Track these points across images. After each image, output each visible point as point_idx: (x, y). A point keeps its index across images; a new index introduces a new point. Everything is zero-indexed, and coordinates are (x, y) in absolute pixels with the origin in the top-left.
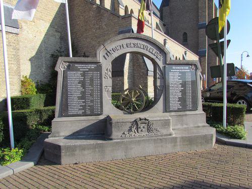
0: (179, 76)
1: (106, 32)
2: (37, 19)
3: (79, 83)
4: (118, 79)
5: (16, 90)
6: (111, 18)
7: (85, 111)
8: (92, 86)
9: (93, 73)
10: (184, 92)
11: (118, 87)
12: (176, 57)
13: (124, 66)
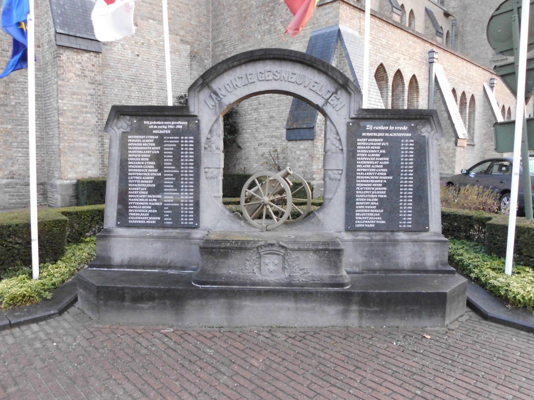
0: (382, 147)
2: (142, 19)
3: (150, 160)
5: (94, 165)
8: (178, 167)
11: (301, 164)
12: (464, 93)
13: (380, 109)
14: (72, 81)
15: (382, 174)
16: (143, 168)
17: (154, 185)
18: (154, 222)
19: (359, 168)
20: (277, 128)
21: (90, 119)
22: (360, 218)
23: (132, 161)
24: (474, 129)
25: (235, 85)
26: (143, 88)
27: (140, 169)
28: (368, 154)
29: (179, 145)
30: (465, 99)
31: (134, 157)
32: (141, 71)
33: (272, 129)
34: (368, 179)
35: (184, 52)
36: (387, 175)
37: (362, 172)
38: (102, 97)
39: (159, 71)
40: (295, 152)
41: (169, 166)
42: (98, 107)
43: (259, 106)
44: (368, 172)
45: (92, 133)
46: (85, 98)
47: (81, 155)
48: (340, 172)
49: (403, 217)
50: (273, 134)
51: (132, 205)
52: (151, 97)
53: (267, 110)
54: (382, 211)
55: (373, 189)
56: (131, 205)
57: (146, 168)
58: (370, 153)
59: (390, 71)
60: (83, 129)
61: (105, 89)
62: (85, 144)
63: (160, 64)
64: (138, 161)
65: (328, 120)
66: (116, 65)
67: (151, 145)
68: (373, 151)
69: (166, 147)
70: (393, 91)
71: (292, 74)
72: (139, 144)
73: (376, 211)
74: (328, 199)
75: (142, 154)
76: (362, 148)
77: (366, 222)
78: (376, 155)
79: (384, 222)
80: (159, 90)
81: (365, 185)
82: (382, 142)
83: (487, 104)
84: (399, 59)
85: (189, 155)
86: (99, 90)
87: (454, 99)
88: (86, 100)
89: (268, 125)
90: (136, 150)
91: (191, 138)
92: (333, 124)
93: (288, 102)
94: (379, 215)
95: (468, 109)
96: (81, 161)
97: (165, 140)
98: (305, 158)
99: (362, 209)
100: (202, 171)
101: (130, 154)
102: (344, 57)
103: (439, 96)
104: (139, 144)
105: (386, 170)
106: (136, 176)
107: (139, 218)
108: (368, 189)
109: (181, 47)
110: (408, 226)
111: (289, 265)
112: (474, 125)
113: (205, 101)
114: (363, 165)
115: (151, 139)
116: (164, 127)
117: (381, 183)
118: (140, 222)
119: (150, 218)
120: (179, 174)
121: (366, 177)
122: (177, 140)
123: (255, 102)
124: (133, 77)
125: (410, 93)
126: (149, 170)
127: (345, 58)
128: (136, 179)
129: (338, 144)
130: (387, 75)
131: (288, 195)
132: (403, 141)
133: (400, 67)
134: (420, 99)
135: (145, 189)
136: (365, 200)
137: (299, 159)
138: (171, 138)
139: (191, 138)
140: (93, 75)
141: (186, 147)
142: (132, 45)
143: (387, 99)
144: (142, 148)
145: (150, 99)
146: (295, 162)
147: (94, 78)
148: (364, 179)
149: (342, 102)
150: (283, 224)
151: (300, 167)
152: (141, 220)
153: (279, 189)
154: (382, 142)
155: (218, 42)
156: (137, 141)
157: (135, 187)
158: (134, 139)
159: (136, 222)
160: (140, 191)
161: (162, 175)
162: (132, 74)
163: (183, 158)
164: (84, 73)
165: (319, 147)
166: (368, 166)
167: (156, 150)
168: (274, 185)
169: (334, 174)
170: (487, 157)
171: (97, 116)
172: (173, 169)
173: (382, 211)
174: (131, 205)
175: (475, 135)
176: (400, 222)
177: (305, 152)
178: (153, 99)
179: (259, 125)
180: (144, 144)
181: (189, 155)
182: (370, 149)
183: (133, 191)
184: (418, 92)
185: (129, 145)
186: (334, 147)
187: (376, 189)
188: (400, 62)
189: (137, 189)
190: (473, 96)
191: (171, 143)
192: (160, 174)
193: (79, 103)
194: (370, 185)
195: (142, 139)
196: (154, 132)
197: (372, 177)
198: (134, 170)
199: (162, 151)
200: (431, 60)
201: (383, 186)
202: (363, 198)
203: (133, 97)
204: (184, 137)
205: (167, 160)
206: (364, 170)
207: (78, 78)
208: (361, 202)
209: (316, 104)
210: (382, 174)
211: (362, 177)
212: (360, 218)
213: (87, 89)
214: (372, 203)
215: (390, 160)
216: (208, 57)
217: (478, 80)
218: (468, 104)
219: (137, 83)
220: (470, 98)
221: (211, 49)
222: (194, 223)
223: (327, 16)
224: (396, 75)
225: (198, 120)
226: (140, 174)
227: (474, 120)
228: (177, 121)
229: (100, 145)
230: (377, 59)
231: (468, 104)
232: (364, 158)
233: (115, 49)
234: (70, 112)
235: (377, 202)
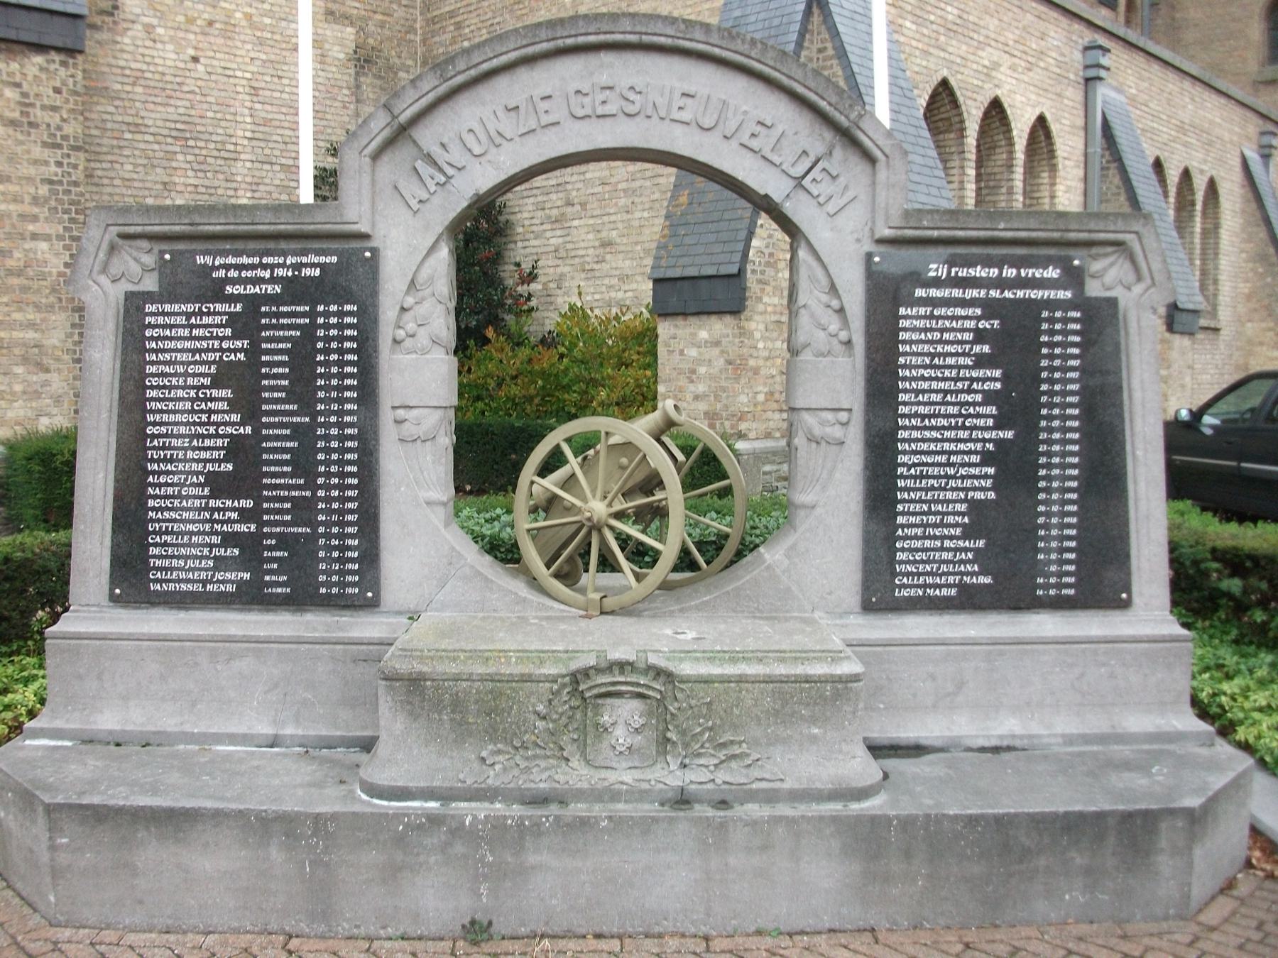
0: (980, 336)
3: (217, 383)
4: (704, 334)
5: (58, 400)
8: (307, 405)
9: (313, 315)
11: (701, 388)
12: (1186, 175)
17: (230, 467)
18: (231, 588)
19: (905, 404)
20: (624, 278)
21: (47, 256)
22: (910, 568)
23: (158, 387)
24: (1216, 282)
25: (493, 134)
26: (209, 160)
27: (183, 412)
28: (932, 356)
29: (309, 333)
30: (1191, 190)
32: (205, 106)
33: (606, 281)
34: (936, 440)
35: (336, 48)
36: (997, 427)
37: (916, 415)
38: (81, 189)
39: (258, 106)
40: (682, 353)
42: (72, 220)
43: (569, 210)
44: (935, 416)
45: (52, 299)
46: (32, 190)
47: (19, 370)
48: (843, 416)
49: (1050, 562)
50: (613, 294)
51: (160, 533)
52: (234, 185)
53: (591, 221)
54: (981, 543)
55: (951, 471)
56: (154, 532)
57: (202, 411)
58: (939, 355)
59: (969, 102)
60: (25, 289)
61: (92, 165)
62: (31, 335)
63: (263, 85)
64: (177, 387)
65: (803, 244)
66: (128, 88)
68: (948, 348)
69: (270, 340)
70: (980, 164)
71: (683, 94)
72: (181, 332)
73: (961, 543)
74: (804, 506)
75: (190, 363)
76: (915, 337)
77: (930, 580)
78: (962, 361)
79: (986, 580)
80: (258, 165)
81: (924, 459)
82: (978, 319)
83: (1254, 206)
84: (996, 66)
86: (75, 167)
87: (1159, 190)
89: (596, 267)
90: (170, 350)
91: (348, 308)
92: (818, 258)
93: (657, 196)
94: (970, 555)
95: (1198, 219)
96: (18, 388)
97: (266, 315)
98: (715, 371)
99: (916, 537)
100: (386, 417)
101: (153, 363)
102: (831, 58)
103: (1117, 180)
104: (181, 332)
105: (992, 410)
106: (172, 436)
108: (936, 471)
109: (328, 33)
110: (1065, 592)
111: (683, 733)
112: (1216, 268)
113: (396, 187)
114: (917, 392)
115: (219, 314)
116: (261, 273)
117: (976, 452)
118: (184, 587)
119: (219, 576)
120: (314, 425)
121: (927, 434)
122: (303, 315)
123: (554, 197)
124: (179, 126)
125: (1030, 171)
126: (214, 418)
127: (835, 62)
128: (170, 448)
130: (961, 114)
131: (673, 494)
132: (1045, 314)
133: (999, 92)
134: (1060, 188)
135: (202, 479)
136: (925, 508)
137: (693, 371)
138: (283, 309)
139: (348, 308)
140: (55, 119)
141: (333, 339)
142: (178, 28)
143: (962, 189)
144: (188, 344)
145: (231, 193)
146: (683, 382)
147: (59, 128)
148: (924, 440)
149: (846, 188)
150: (659, 588)
151: (696, 398)
152: (188, 581)
153: (639, 476)
154: (978, 319)
155: (441, 18)
156: (173, 320)
157: (168, 473)
158: (164, 314)
159: (171, 587)
160: (183, 485)
162: (176, 117)
163: (321, 376)
164: (27, 114)
165: (757, 335)
166: (934, 397)
168: (624, 461)
169: (823, 423)
170: (1257, 366)
171: (67, 248)
172: (291, 414)
173: (981, 543)
174: (154, 532)
175: (1221, 298)
176: (1040, 580)
177: (716, 351)
178: (240, 193)
179: (566, 269)
180: (196, 332)
182: (940, 341)
183: (160, 485)
184: (1053, 169)
185: (148, 333)
186: (822, 334)
187: (963, 471)
188: (1000, 76)
189: (176, 479)
191: (283, 327)
192: (249, 430)
193: (12, 207)
195: (188, 316)
196: (229, 289)
197: (947, 434)
198: (165, 417)
199: (254, 352)
200: (1092, 73)
201: (983, 463)
202: (921, 501)
203: (179, 188)
204: (327, 305)
205: (272, 382)
207: (11, 131)
208: (915, 514)
209: (762, 192)
211: (916, 434)
212: (910, 568)
213: (36, 162)
214: (950, 519)
215: (1005, 379)
216: (410, 62)
217: (1227, 136)
218: (1199, 207)
219: (191, 143)
221: (418, 39)
224: (986, 115)
225: (374, 251)
226: (183, 430)
227: (1216, 254)
228: (304, 253)
230: (932, 66)
231: (1199, 207)
232: (921, 371)
233: (127, 40)
235: (962, 514)
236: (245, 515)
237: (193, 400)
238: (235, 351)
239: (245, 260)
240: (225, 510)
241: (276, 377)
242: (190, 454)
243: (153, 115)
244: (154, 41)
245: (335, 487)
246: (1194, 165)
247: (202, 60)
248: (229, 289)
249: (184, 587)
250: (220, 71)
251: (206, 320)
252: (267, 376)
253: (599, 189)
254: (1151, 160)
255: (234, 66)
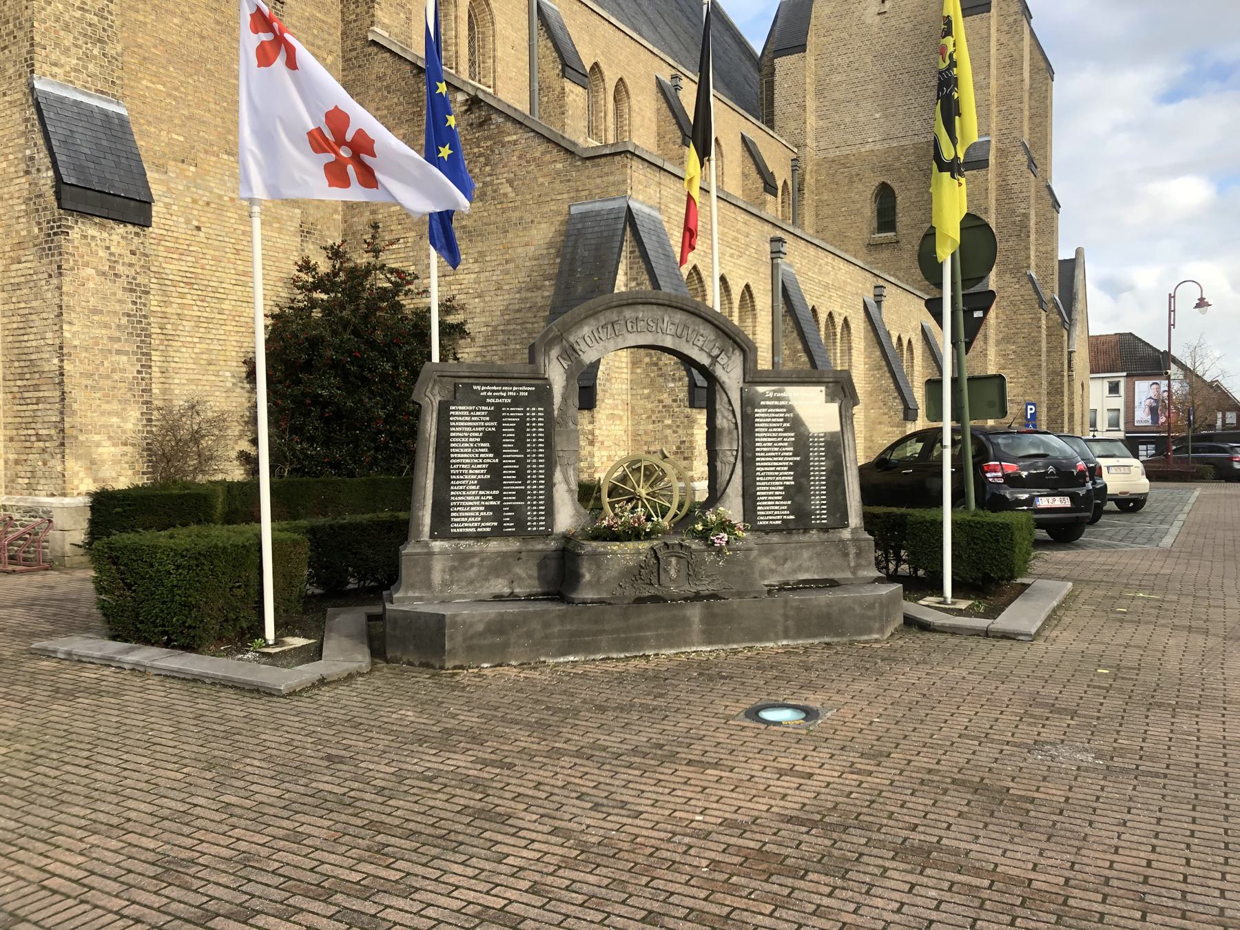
1: (515, 215)
6: (538, 154)
7: (501, 523)
8: (523, 450)
10: (801, 470)
12: (830, 315)
14: (91, 285)
15: (787, 454)
16: (472, 453)
18: (488, 529)
28: (768, 428)
31: (458, 437)
41: (510, 448)
51: (457, 506)
54: (789, 502)
67: (484, 418)
72: (467, 418)
85: (537, 432)
88: (118, 326)
97: (504, 412)
104: (467, 418)
105: (792, 449)
107: (466, 525)
114: (763, 442)
118: (467, 530)
129: (731, 417)
144: (470, 424)
147: (135, 279)
156: (463, 413)
157: (460, 480)
158: (459, 410)
161: (500, 461)
167: (492, 426)
171: (139, 360)
181: (537, 432)
190: (846, 320)
191: (512, 417)
193: (104, 332)
194: (773, 469)
195: (470, 411)
196: (488, 400)
199: (499, 427)
206: (765, 449)
210: (787, 454)
211: (763, 459)
214: (777, 493)
220: (842, 322)
222: (547, 529)
223: (605, 179)
226: (468, 461)
228: (521, 385)
229: (144, 422)
234: (86, 351)
236: (495, 498)
237: (472, 448)
238: (491, 427)
239: (495, 388)
240: (486, 495)
241: (509, 438)
242: (471, 471)
243: (171, 266)
244: (171, 215)
245: (535, 484)
246: (836, 309)
247: (203, 229)
248: (488, 400)
249: (467, 530)
250: (214, 237)
251: (478, 413)
252: (505, 438)
253: (485, 329)
254: (810, 308)
255: (224, 234)
